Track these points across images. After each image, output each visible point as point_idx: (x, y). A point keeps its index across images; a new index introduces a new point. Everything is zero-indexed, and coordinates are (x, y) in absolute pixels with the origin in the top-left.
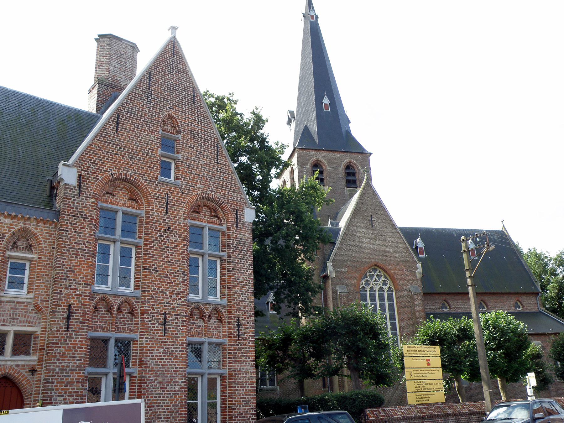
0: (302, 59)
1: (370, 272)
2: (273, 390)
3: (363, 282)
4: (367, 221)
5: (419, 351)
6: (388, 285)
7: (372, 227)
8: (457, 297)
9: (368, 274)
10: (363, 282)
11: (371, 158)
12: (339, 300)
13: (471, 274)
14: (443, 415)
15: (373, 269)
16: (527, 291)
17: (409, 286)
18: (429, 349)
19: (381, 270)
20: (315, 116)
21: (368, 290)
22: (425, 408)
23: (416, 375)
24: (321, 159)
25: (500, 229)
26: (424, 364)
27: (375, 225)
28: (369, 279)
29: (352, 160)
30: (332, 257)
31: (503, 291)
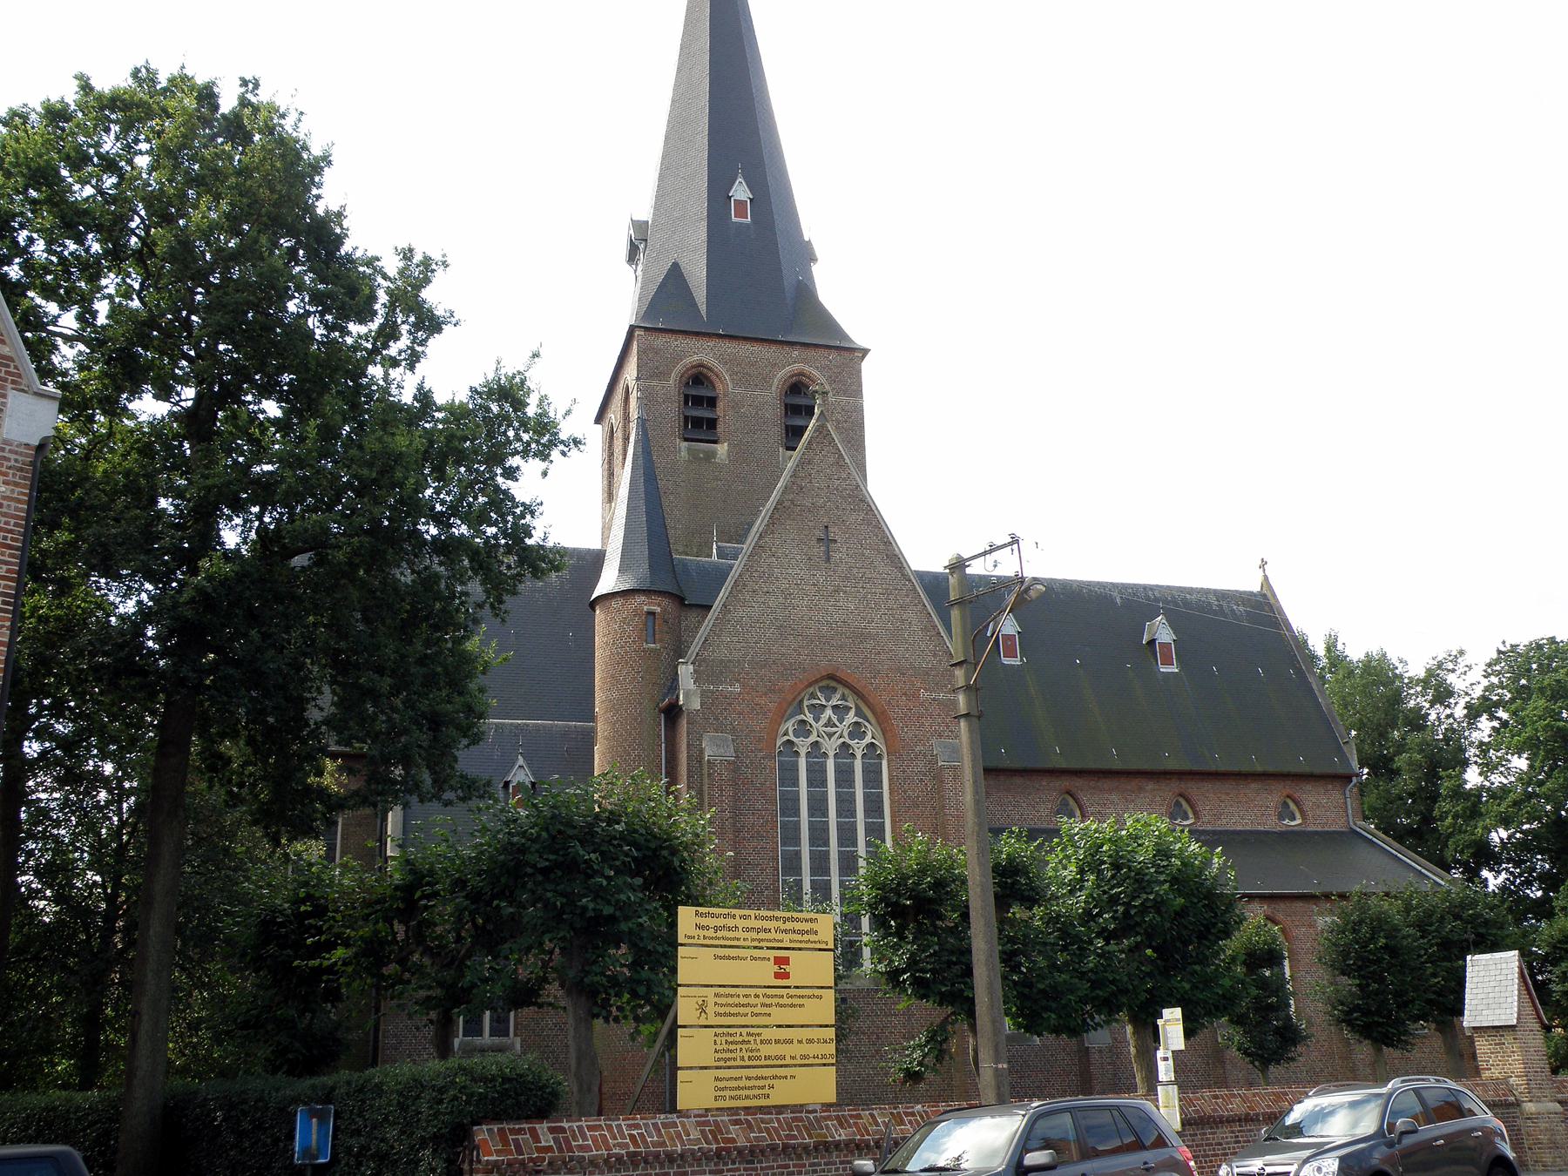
0: (679, 70)
1: (813, 696)
2: (500, 1049)
3: (790, 725)
4: (814, 542)
5: (748, 930)
6: (868, 739)
7: (828, 560)
8: (1107, 784)
9: (806, 703)
10: (790, 725)
11: (867, 366)
12: (706, 780)
13: (968, 678)
14: (805, 1148)
15: (821, 689)
16: (1317, 771)
17: (933, 741)
18: (789, 925)
19: (847, 692)
20: (703, 235)
21: (803, 752)
22: (736, 1122)
23: (722, 1010)
24: (710, 360)
25: (1256, 588)
26: (764, 972)
27: (836, 556)
28: (809, 718)
29: (807, 369)
30: (694, 649)
31: (1245, 768)
